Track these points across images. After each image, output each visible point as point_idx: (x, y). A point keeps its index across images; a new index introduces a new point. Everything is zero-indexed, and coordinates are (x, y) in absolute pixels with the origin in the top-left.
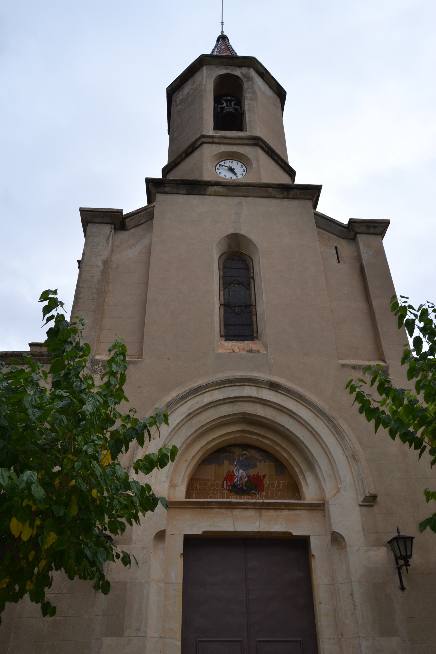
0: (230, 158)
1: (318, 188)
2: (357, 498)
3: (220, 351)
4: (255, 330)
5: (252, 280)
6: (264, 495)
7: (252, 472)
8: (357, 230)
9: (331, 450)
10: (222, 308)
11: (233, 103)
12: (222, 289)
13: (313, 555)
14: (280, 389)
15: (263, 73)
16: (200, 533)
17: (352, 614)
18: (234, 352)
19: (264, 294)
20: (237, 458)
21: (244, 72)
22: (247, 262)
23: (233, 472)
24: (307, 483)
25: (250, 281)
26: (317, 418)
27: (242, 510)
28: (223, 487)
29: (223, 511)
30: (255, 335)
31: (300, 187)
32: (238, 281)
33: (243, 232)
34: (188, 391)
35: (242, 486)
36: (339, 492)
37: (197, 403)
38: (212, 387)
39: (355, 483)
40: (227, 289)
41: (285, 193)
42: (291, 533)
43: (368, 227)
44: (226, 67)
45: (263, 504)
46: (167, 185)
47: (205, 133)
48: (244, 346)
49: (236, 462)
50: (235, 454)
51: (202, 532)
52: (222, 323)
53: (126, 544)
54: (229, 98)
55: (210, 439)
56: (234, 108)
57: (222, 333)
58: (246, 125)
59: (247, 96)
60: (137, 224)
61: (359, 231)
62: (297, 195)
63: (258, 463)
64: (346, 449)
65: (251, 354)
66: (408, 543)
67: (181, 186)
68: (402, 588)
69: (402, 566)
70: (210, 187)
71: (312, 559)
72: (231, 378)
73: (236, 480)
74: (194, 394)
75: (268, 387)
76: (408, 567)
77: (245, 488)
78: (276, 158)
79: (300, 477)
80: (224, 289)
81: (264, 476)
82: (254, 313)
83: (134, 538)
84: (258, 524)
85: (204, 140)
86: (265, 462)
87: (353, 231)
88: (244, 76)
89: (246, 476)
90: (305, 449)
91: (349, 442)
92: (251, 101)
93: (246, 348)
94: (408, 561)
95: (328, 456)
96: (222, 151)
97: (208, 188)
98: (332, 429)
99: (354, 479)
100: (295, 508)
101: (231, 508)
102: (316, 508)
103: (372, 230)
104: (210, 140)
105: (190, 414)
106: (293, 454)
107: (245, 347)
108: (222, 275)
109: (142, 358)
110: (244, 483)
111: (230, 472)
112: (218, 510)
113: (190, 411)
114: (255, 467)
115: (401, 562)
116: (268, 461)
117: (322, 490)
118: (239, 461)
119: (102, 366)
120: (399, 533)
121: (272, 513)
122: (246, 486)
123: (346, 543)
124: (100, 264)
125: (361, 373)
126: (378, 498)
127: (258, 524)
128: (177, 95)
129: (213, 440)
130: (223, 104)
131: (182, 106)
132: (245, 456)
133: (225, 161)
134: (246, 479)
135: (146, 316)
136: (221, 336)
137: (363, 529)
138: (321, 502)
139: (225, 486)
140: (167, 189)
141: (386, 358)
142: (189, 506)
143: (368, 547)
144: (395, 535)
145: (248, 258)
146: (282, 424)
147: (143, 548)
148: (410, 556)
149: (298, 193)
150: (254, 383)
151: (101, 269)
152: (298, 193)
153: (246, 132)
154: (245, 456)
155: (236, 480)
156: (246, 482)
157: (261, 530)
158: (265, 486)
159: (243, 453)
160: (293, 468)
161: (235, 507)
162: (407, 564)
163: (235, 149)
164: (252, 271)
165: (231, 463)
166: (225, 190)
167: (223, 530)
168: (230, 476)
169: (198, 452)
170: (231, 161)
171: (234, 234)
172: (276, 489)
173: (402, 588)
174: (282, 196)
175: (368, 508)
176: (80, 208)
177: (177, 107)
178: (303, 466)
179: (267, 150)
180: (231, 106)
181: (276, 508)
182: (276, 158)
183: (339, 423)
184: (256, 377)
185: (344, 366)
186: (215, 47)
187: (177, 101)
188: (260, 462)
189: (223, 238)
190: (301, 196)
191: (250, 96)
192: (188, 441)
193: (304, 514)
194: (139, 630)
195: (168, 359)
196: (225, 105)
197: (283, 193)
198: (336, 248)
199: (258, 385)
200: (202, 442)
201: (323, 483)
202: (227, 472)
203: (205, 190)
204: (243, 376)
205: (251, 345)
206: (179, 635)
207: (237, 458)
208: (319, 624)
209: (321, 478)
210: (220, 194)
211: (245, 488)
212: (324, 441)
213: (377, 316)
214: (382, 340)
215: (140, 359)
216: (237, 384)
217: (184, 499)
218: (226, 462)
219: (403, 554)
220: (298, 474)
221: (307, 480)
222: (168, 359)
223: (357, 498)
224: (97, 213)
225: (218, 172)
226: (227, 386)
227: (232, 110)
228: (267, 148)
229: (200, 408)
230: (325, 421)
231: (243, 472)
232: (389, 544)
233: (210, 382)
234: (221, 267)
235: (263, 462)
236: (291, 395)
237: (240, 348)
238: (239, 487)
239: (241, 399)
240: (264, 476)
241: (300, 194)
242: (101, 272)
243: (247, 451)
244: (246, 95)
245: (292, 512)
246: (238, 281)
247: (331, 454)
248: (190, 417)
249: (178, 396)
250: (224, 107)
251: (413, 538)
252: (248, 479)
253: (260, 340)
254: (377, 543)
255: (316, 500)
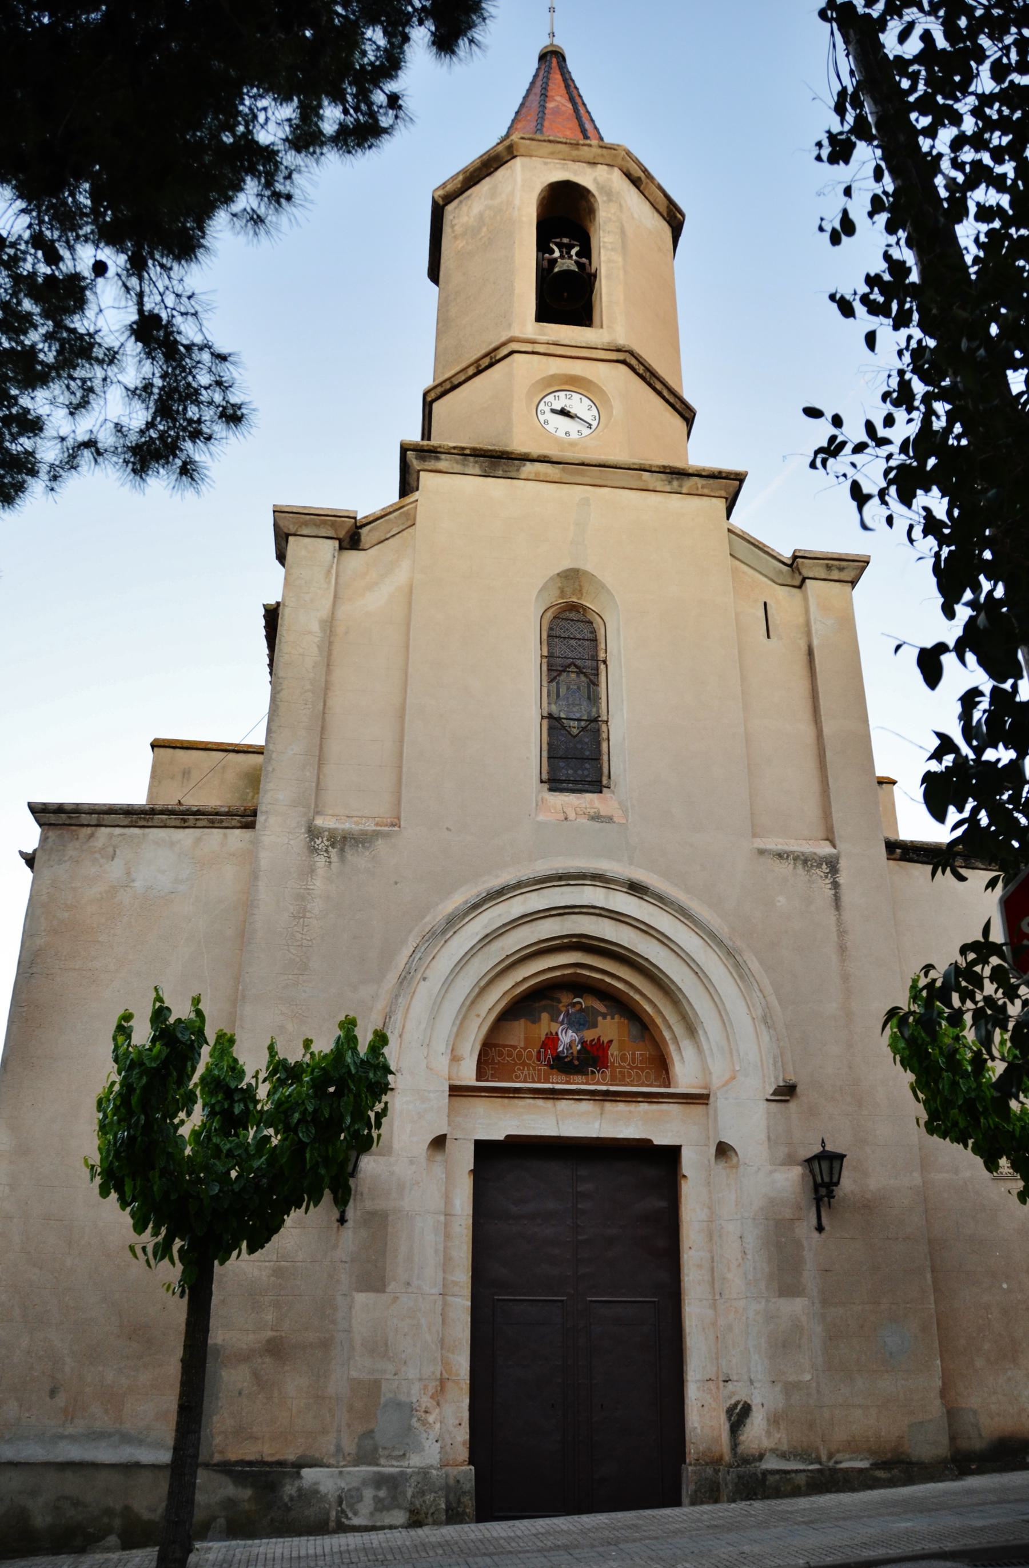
0: (567, 387)
1: (739, 478)
2: (764, 1088)
3: (541, 818)
4: (605, 771)
5: (602, 667)
6: (608, 1074)
7: (589, 1035)
8: (806, 573)
9: (728, 1006)
10: (545, 722)
11: (573, 252)
12: (545, 683)
13: (685, 1176)
14: (646, 894)
15: (639, 178)
16: (502, 1138)
17: (739, 1266)
18: (566, 819)
19: (625, 703)
20: (563, 1009)
21: (600, 179)
22: (594, 625)
23: (557, 1034)
24: (682, 1058)
25: (597, 669)
26: (708, 948)
27: (572, 1102)
28: (539, 1059)
29: (540, 1102)
30: (605, 782)
31: (704, 474)
32: (576, 666)
33: (589, 568)
34: (484, 894)
35: (572, 1059)
36: (733, 1078)
37: (500, 915)
38: (526, 887)
39: (762, 1065)
40: (554, 684)
41: (675, 483)
42: (650, 1141)
43: (829, 568)
44: (564, 164)
45: (607, 1093)
46: (443, 456)
47: (516, 333)
48: (584, 806)
49: (562, 1017)
50: (561, 1002)
51: (504, 1136)
52: (545, 754)
53: (384, 1155)
54: (565, 240)
55: (521, 979)
56: (576, 262)
57: (545, 777)
58: (601, 294)
59: (606, 240)
60: (383, 538)
61: (811, 575)
62: (697, 489)
63: (600, 1019)
64: (754, 1006)
65: (597, 825)
66: (836, 1165)
67: (471, 459)
68: (820, 1228)
69: (824, 1196)
70: (528, 463)
71: (683, 1182)
72: (560, 871)
73: (560, 1049)
74: (495, 899)
75: (625, 890)
76: (832, 1200)
77: (576, 1063)
78: (659, 386)
79: (672, 1048)
80: (550, 681)
81: (611, 1041)
82: (604, 736)
83: (396, 1146)
84: (597, 1125)
85: (515, 346)
86: (613, 1018)
87: (800, 573)
88: (601, 188)
89: (580, 1040)
90: (684, 1001)
91: (759, 994)
92: (613, 253)
93: (588, 810)
94: (832, 1191)
95: (721, 1015)
96: (551, 372)
97: (524, 465)
98: (732, 970)
99: (761, 1057)
100: (661, 1100)
101: (553, 1099)
102: (694, 1101)
103: (835, 575)
104: (528, 347)
105: (487, 936)
106: (662, 1009)
107: (586, 808)
108: (546, 654)
109: (399, 827)
110: (575, 1054)
111: (551, 1033)
112: (531, 1101)
113: (488, 931)
114: (595, 1025)
115: (823, 1191)
116: (616, 1016)
117: (705, 1070)
118: (567, 1014)
119: (328, 840)
120: (823, 1147)
121: (621, 1107)
122: (578, 1059)
123: (738, 1161)
124: (315, 627)
125: (791, 866)
126: (798, 1089)
127: (597, 1125)
128: (457, 211)
129: (525, 979)
130: (553, 252)
131: (467, 243)
132: (578, 1007)
133: (557, 394)
134: (579, 1047)
135: (405, 740)
136: (542, 782)
137: (769, 1138)
138: (704, 1092)
139: (542, 1058)
140: (442, 465)
141: (836, 838)
142: (483, 1094)
143: (774, 1167)
144: (817, 1149)
145: (597, 617)
146: (646, 956)
147: (411, 1162)
148: (837, 1183)
149: (700, 486)
150: (601, 882)
151: (318, 639)
152: (700, 486)
153: (601, 330)
154: (578, 1007)
155: (560, 1049)
156: (579, 1052)
157: (602, 1135)
158: (611, 1059)
159: (575, 1000)
160: (661, 1032)
161: (560, 1097)
162: (830, 1195)
163: (577, 368)
164: (603, 646)
165: (554, 1019)
166: (557, 471)
167: (539, 1134)
168: (552, 1040)
169: (498, 1000)
170: (568, 393)
171: (571, 570)
172: (629, 1065)
173: (820, 1228)
174: (668, 488)
175: (779, 1105)
176: (277, 511)
177: (457, 242)
178: (679, 1029)
179: (641, 372)
180: (570, 257)
181: (629, 1099)
182: (659, 386)
183: (745, 958)
184: (606, 871)
185: (762, 852)
186: (536, 76)
187: (456, 228)
188: (604, 1018)
189: (552, 579)
190: (706, 491)
191: (611, 241)
192: (482, 983)
193: (674, 1109)
194: (408, 1284)
195: (448, 829)
196: (557, 254)
197: (670, 482)
198: (765, 604)
199: (608, 886)
200: (506, 984)
201: (709, 1060)
202: (547, 1034)
203: (518, 470)
204: (583, 868)
205: (597, 804)
206: (467, 1291)
207: (563, 1009)
208: (686, 1279)
209: (707, 1052)
210: (548, 479)
211: (576, 1063)
212: (714, 986)
213: (828, 754)
214: (833, 804)
215: (396, 828)
216: (572, 882)
217: (474, 1083)
218: (545, 1016)
219: (826, 1179)
220: (669, 1042)
221: (683, 1054)
222: (448, 829)
223: (764, 1088)
224: (308, 517)
225: (542, 418)
226: (554, 886)
227: (575, 268)
228: (642, 368)
229: (504, 925)
230: (720, 954)
231: (574, 1034)
232: (806, 1164)
233: (523, 879)
234: (545, 636)
235: (609, 1018)
236: (666, 906)
237: (578, 809)
238: (566, 1060)
239: (577, 910)
240: (611, 1041)
241: (702, 487)
242: (318, 646)
243: (581, 998)
244: (604, 237)
245: (654, 1107)
246: (576, 666)
247: (727, 1014)
248: (487, 940)
249: (466, 902)
250: (555, 261)
251: (845, 1156)
252: (582, 1047)
253: (613, 792)
254: (789, 1160)
255: (693, 1087)
